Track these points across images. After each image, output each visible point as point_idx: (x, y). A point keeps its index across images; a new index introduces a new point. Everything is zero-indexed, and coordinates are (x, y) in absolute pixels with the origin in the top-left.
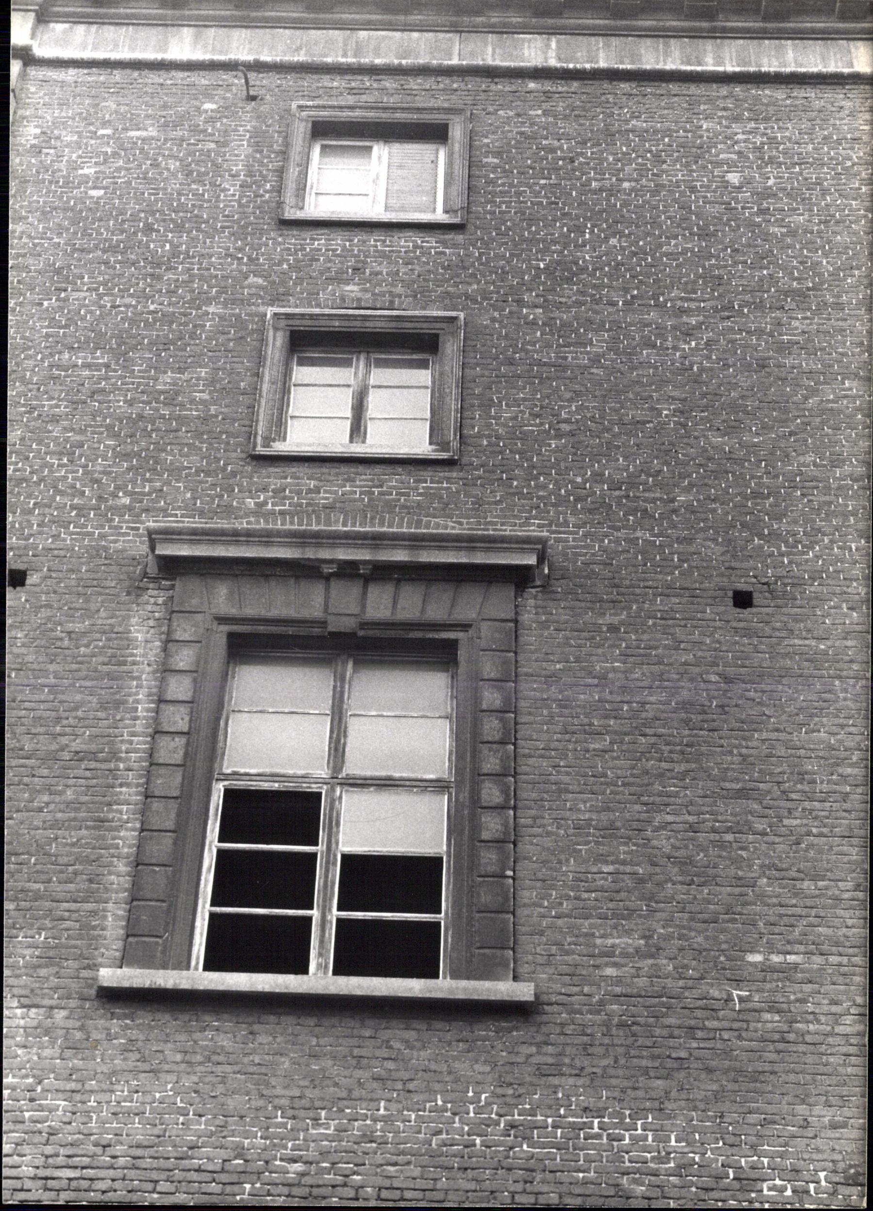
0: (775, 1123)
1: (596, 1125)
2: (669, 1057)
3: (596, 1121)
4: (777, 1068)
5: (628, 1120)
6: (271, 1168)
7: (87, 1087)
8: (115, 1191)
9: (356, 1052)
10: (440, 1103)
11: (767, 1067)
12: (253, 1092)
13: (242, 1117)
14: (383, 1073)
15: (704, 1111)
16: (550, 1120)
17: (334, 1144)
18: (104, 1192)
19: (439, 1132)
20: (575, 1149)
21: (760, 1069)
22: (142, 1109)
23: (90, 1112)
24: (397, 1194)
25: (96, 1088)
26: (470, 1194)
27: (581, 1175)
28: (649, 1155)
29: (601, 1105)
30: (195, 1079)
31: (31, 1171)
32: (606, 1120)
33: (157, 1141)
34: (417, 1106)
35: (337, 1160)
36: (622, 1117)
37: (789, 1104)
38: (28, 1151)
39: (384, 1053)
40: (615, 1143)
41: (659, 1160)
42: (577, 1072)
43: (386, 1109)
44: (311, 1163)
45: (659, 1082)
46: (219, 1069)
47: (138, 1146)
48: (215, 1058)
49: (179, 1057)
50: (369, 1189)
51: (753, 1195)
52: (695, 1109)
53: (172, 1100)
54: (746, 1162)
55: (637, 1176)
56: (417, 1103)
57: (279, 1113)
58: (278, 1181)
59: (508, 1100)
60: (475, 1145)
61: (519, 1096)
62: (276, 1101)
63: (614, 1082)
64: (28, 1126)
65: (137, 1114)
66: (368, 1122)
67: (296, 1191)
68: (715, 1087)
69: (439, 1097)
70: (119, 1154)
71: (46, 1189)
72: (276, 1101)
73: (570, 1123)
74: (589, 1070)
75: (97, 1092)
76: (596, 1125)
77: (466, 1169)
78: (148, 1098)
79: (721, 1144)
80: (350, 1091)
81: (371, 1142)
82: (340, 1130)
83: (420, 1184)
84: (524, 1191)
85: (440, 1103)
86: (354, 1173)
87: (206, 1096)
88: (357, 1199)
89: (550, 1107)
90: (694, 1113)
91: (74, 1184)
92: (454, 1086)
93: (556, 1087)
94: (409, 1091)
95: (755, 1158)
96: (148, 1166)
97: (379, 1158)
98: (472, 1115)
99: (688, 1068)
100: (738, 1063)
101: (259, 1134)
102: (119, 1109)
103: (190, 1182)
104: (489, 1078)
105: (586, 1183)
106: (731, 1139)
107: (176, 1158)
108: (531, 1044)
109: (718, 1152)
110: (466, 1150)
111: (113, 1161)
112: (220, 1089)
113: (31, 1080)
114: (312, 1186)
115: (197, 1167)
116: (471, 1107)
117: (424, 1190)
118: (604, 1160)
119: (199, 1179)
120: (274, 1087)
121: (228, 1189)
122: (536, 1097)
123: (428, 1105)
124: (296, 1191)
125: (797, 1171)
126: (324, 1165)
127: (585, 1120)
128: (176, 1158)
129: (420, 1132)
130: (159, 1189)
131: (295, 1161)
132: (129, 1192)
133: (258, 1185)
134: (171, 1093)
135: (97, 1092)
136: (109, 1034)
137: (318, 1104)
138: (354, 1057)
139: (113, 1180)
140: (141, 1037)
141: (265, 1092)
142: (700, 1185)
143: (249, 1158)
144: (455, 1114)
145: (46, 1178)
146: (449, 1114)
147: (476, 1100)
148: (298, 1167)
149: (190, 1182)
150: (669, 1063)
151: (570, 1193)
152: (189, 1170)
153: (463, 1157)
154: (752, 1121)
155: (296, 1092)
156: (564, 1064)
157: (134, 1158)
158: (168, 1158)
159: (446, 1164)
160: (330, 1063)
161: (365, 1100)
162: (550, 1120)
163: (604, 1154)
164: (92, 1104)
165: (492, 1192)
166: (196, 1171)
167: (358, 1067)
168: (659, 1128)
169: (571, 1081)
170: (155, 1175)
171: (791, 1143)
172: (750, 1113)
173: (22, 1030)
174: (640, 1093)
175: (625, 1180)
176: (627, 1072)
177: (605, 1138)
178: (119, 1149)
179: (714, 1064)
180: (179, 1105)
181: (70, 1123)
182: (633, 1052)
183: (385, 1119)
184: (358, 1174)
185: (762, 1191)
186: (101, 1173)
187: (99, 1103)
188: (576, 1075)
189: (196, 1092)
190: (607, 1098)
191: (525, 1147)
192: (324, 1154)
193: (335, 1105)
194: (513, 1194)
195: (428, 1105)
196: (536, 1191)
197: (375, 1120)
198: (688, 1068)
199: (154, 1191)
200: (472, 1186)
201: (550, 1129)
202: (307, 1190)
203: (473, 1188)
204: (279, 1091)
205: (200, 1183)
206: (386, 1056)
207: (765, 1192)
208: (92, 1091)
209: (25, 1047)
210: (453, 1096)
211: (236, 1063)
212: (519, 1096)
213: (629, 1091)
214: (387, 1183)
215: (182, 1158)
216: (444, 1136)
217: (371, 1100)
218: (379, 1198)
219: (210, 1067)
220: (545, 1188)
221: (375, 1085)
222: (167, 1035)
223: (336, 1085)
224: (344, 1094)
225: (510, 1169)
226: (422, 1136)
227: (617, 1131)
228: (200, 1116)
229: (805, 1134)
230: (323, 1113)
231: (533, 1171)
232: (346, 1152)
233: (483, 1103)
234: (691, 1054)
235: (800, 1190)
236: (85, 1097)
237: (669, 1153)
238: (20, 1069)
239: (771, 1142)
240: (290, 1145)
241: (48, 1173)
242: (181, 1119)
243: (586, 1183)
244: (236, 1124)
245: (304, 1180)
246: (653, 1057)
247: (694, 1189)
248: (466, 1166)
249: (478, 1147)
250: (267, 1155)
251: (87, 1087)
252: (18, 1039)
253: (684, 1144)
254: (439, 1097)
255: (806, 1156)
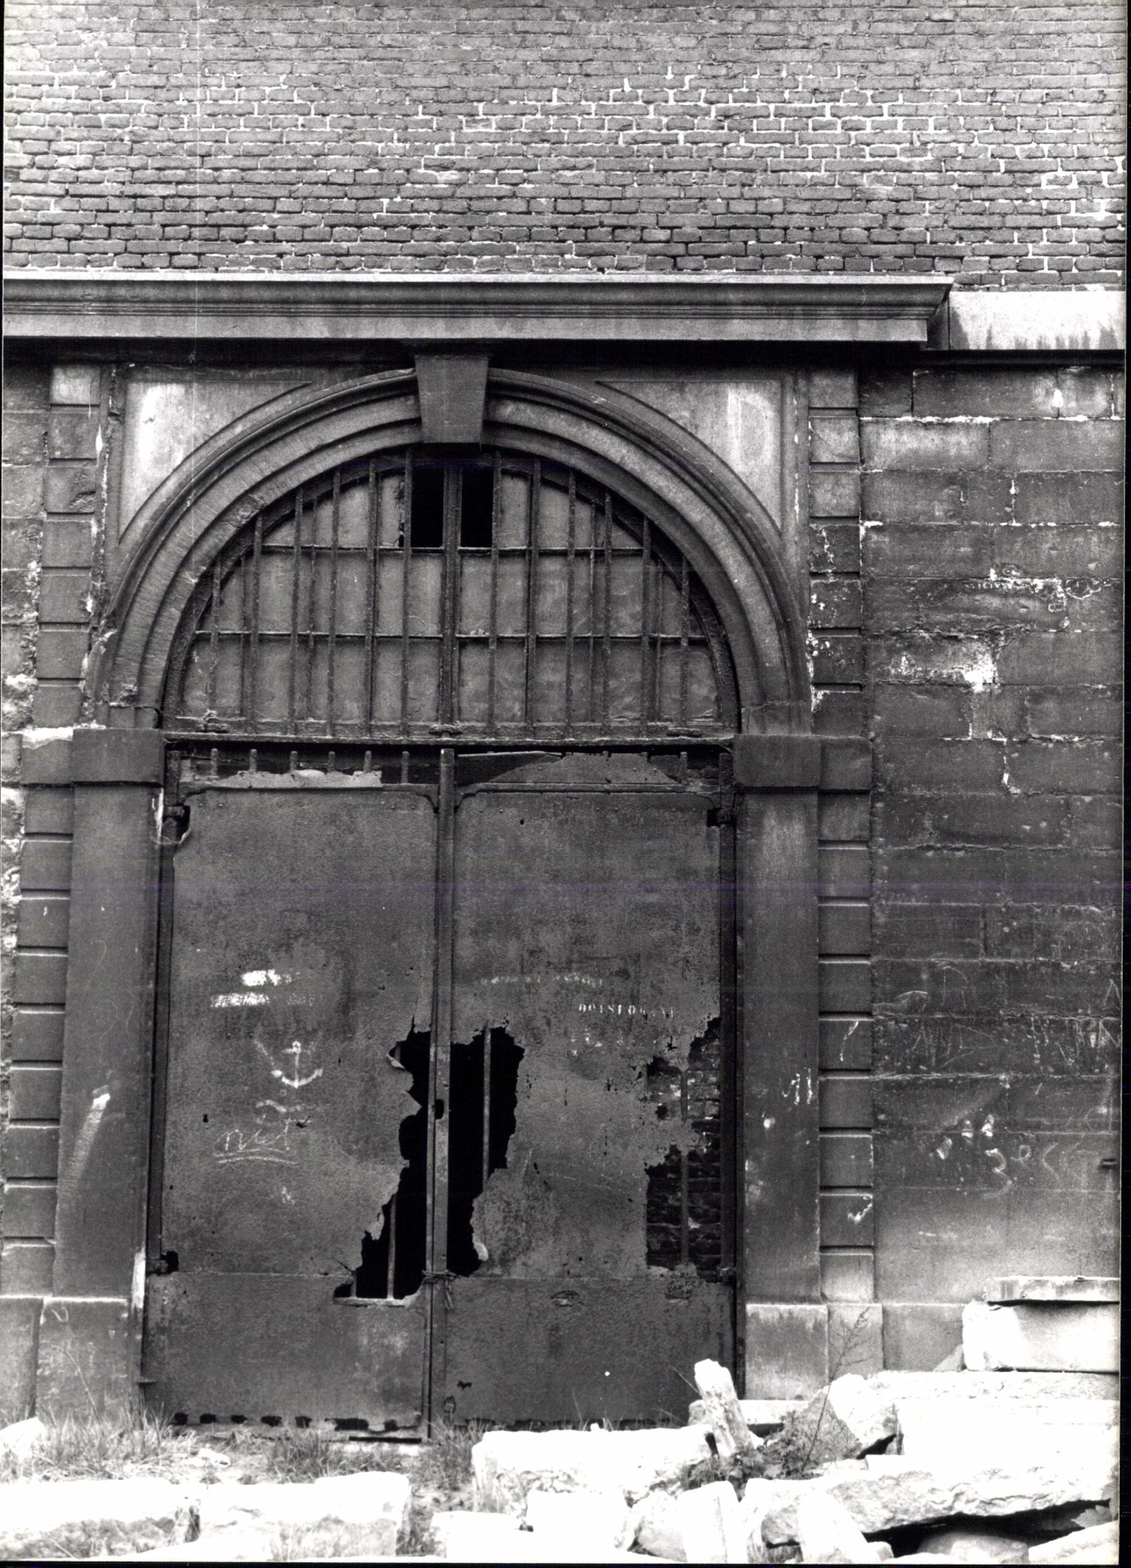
0: (1059, 98)
1: (828, 112)
2: (928, 19)
3: (828, 106)
4: (1070, 26)
5: (870, 103)
6: (413, 177)
7: (173, 81)
8: (222, 210)
9: (520, 25)
10: (627, 89)
11: (1053, 27)
12: (383, 83)
13: (372, 115)
14: (555, 52)
15: (971, 88)
16: (772, 107)
17: (497, 145)
18: (207, 212)
19: (628, 127)
20: (801, 143)
21: (1044, 30)
22: (247, 108)
23: (179, 113)
24: (576, 206)
25: (185, 83)
26: (670, 202)
27: (809, 175)
28: (897, 147)
29: (834, 85)
30: (314, 67)
31: (117, 189)
32: (841, 104)
33: (272, 147)
34: (598, 94)
35: (503, 165)
36: (862, 100)
37: (1079, 73)
38: (108, 163)
39: (553, 26)
40: (853, 134)
41: (911, 152)
42: (805, 43)
43: (560, 99)
44: (468, 170)
45: (914, 53)
46: (342, 54)
47: (248, 155)
48: (336, 40)
49: (292, 40)
50: (543, 200)
51: (1029, 190)
52: (960, 86)
53: (288, 96)
54: (1023, 151)
55: (882, 173)
56: (598, 89)
57: (420, 108)
58: (423, 193)
59: (722, 82)
60: (677, 142)
61: (735, 77)
62: (415, 94)
63: (852, 54)
64: (106, 131)
65: (240, 115)
66: (539, 116)
67: (449, 205)
68: (986, 56)
69: (626, 81)
70: (221, 165)
71: (137, 210)
72: (415, 94)
73: (795, 110)
74: (820, 40)
75: (186, 87)
76: (828, 112)
77: (665, 171)
78: (255, 94)
79: (991, 127)
80: (514, 77)
81: (543, 141)
82: (505, 127)
83: (606, 191)
84: (742, 197)
85: (627, 89)
86: (524, 181)
87: (328, 90)
88: (529, 213)
89: (772, 89)
90: (958, 91)
91: (169, 203)
92: (646, 66)
93: (779, 63)
94: (588, 75)
95: (1034, 145)
96: (263, 180)
97: (554, 161)
98: (672, 102)
99: (953, 33)
100: (1016, 24)
101: (396, 136)
102: (217, 110)
103: (318, 198)
104: (695, 54)
105: (815, 185)
106: (1003, 122)
107: (298, 169)
108: (749, 8)
109: (987, 139)
110: (665, 148)
111: (216, 174)
112: (345, 79)
113: (102, 73)
114: (471, 199)
115: (324, 179)
116: (671, 93)
117: (610, 199)
118: (838, 155)
119: (329, 194)
120: (411, 75)
121: (364, 205)
122: (756, 77)
123: (612, 92)
124: (449, 205)
125: (1086, 158)
126: (486, 171)
127: (814, 105)
128: (298, 169)
129: (602, 127)
130: (279, 207)
131: (446, 168)
132: (240, 211)
133: (398, 199)
134: (285, 87)
135: (186, 87)
136: (193, 13)
137: (472, 95)
138: (517, 33)
139: (218, 198)
140: (239, 15)
141: (399, 83)
142: (962, 181)
143: (385, 165)
144: (648, 102)
145: (135, 196)
146: (640, 102)
147: (677, 85)
148: (452, 175)
149: (318, 198)
150: (928, 27)
151: (796, 198)
152: (316, 183)
153: (660, 156)
154: (1032, 99)
155: (442, 81)
156: (788, 34)
157: (243, 170)
158: (288, 169)
159: (638, 166)
160: (488, 41)
161: (534, 88)
162: (772, 107)
163: (838, 147)
164: (181, 103)
165: (701, 199)
166: (324, 184)
167: (523, 46)
168: (912, 110)
169: (798, 55)
170: (273, 191)
171: (1080, 124)
172: (1029, 87)
173: (82, 8)
174: (888, 68)
175: (865, 180)
176: (870, 41)
177: (839, 126)
178: (222, 160)
179: (986, 25)
180: (297, 101)
181: (156, 128)
182: (878, 15)
183: (559, 112)
184: (530, 182)
185: (1039, 185)
186: (198, 189)
187: (190, 101)
188: (804, 47)
189: (316, 85)
190: (843, 76)
191: (742, 141)
192: (485, 158)
193: (498, 96)
194: (728, 200)
195: (612, 92)
196: (755, 195)
197: (547, 113)
198: (953, 33)
199: (273, 210)
200: (674, 192)
201: (772, 118)
202: (465, 203)
203: (676, 195)
204: (418, 81)
205: (330, 198)
206: (557, 29)
207: (1044, 187)
208: (179, 87)
209: (90, 30)
210: (643, 79)
211: (361, 46)
212: (735, 77)
213: (872, 67)
214: (564, 191)
215: (305, 169)
216: (634, 131)
217: (541, 88)
218: (556, 211)
219: (330, 51)
220: (766, 192)
221: (544, 68)
222: (273, 11)
223: (496, 70)
224: (507, 81)
225: (723, 170)
226: (605, 132)
227: (855, 118)
228: (324, 115)
229: (1099, 111)
230: (481, 106)
231: (751, 171)
232: (514, 155)
233: (686, 88)
234: (956, 15)
235: (1089, 180)
236: (171, 95)
237: (926, 143)
238: (86, 59)
239: (1054, 124)
240: (437, 148)
241: (137, 189)
242: (301, 120)
243: (815, 185)
244: (365, 124)
245: (459, 192)
246: (906, 20)
247: (955, 187)
248: (664, 167)
249: (681, 143)
250: (408, 162)
251: (173, 81)
252: (79, 19)
253: (945, 131)
254: (626, 81)
255: (1098, 139)
